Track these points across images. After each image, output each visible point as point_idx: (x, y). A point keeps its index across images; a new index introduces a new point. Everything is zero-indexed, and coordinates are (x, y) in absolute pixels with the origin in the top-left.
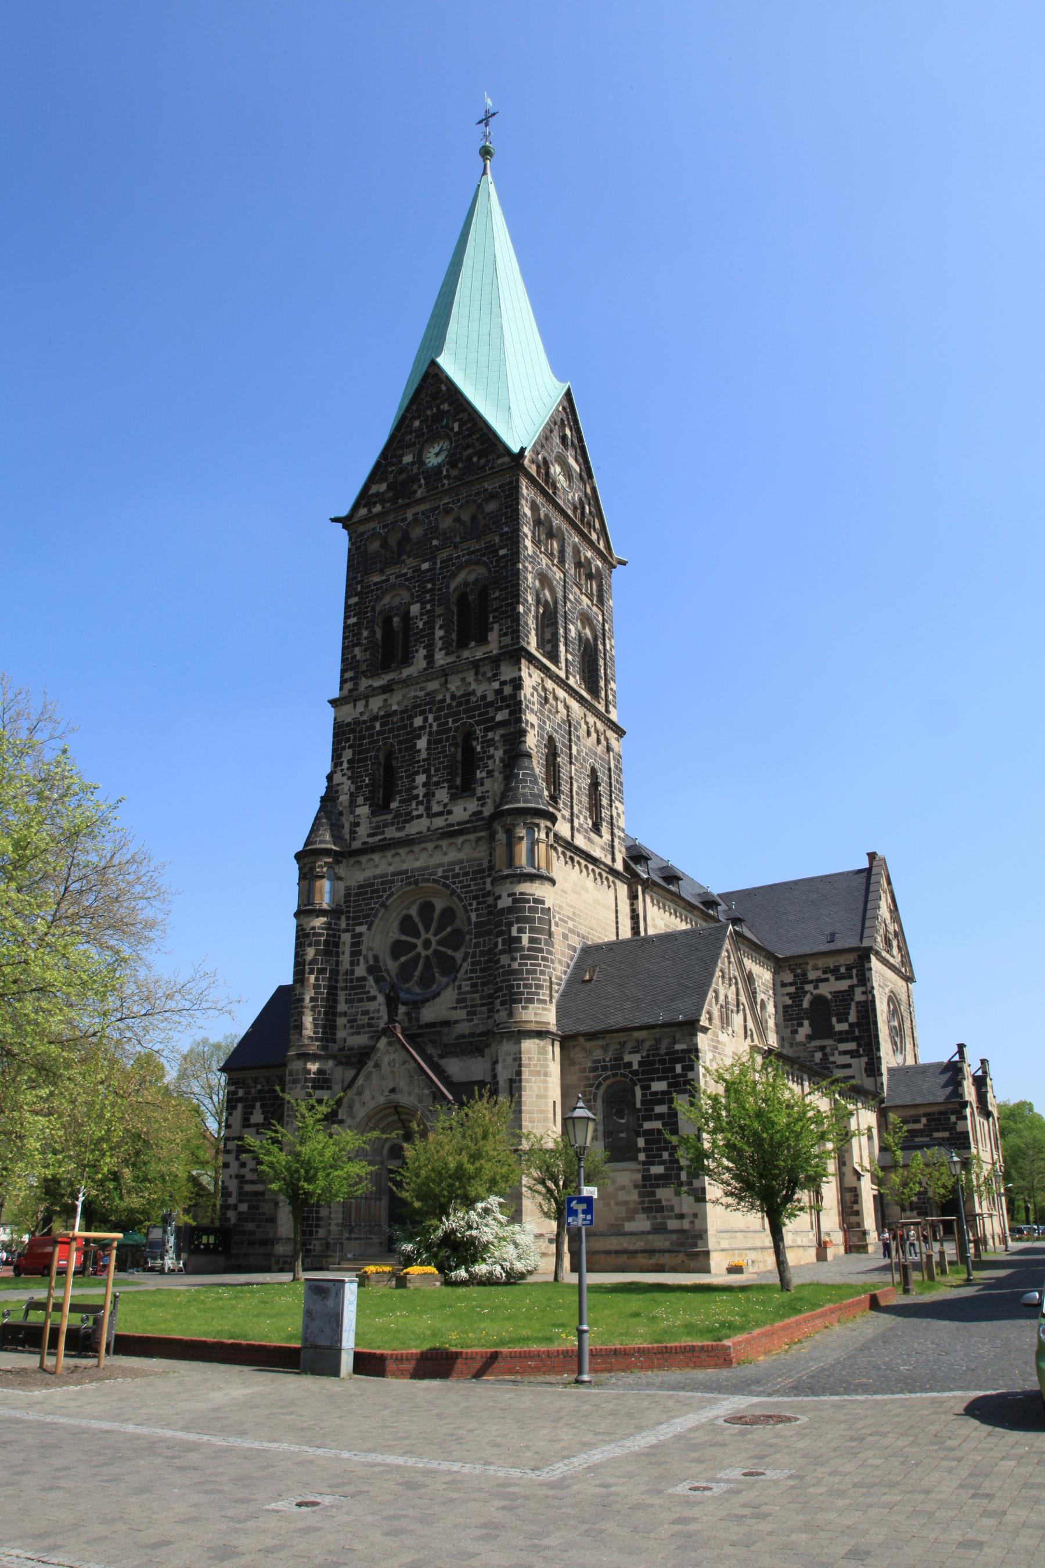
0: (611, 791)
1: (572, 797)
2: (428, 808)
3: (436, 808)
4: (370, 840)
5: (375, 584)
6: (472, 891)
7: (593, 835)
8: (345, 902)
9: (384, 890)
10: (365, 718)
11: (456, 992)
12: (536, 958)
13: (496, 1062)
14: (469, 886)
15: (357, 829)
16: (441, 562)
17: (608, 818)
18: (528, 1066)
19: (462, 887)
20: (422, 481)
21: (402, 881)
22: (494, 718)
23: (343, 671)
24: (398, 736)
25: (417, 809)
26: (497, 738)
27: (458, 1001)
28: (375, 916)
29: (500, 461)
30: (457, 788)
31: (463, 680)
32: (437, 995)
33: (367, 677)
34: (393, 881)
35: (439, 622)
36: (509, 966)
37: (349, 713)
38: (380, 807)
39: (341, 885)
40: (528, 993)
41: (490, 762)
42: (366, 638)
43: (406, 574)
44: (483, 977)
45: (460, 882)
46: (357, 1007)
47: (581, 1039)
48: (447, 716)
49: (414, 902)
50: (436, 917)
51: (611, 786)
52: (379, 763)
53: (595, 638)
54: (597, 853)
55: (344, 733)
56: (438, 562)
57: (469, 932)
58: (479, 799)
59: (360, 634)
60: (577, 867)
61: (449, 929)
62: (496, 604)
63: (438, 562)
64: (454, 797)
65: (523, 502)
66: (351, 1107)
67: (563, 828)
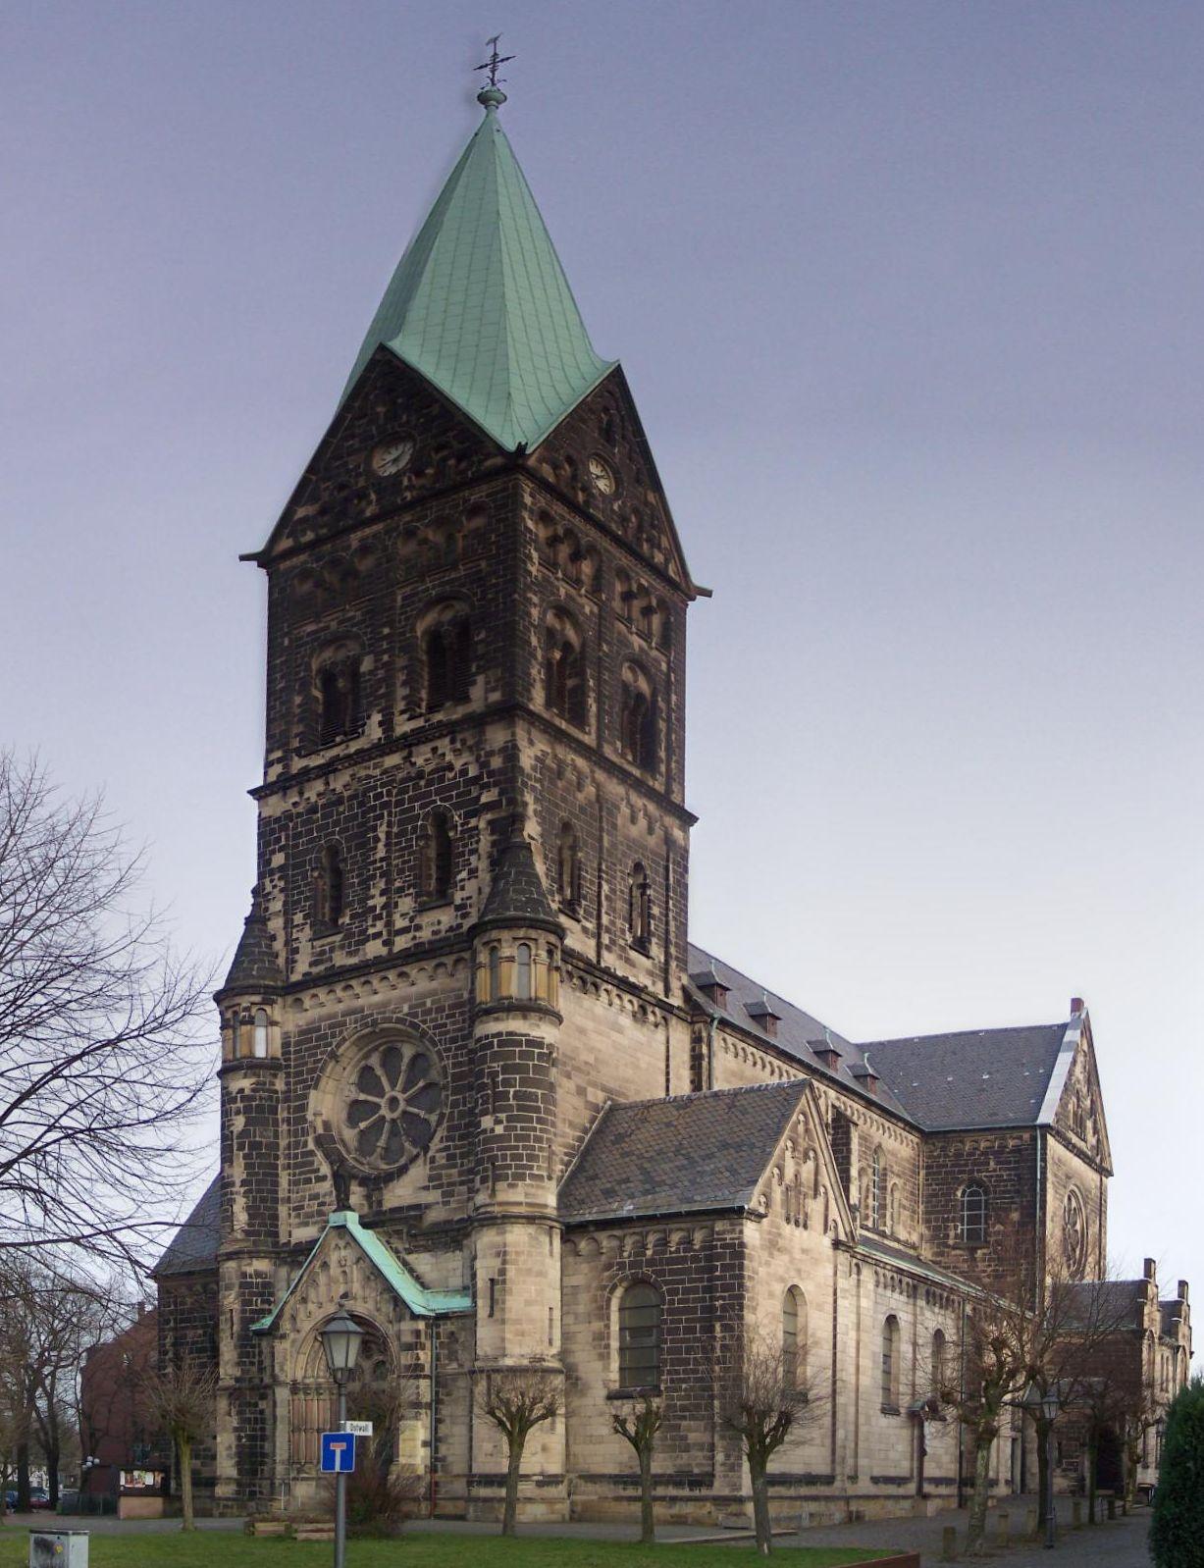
0: (667, 896)
1: (600, 904)
2: (389, 924)
3: (400, 923)
4: (315, 970)
5: (309, 634)
6: (448, 1032)
7: (633, 955)
8: (283, 1054)
9: (333, 1036)
10: (300, 809)
11: (428, 1166)
12: (530, 1119)
13: (474, 1258)
14: (445, 1025)
15: (297, 957)
16: (404, 599)
17: (661, 931)
18: (515, 1262)
19: (435, 1028)
20: (373, 497)
21: (356, 1022)
22: (478, 798)
23: (269, 751)
24: (347, 830)
25: (374, 926)
26: (482, 825)
27: (431, 1179)
28: (322, 1070)
29: (489, 463)
30: (429, 894)
31: (434, 750)
32: (403, 1170)
33: (300, 756)
34: (344, 1024)
35: (401, 677)
36: (493, 1130)
37: (277, 806)
38: (325, 927)
39: (277, 1031)
40: (518, 1167)
41: (473, 859)
42: (299, 706)
43: (353, 617)
44: (463, 1146)
45: (432, 1021)
46: (304, 1190)
47: (592, 1229)
48: (412, 800)
49: (376, 1049)
50: (403, 1068)
51: (667, 890)
52: (323, 869)
53: (654, 694)
54: (641, 979)
55: (273, 831)
56: (399, 598)
57: (445, 1087)
58: (458, 908)
59: (290, 701)
60: (603, 994)
61: (421, 1084)
62: (481, 649)
63: (399, 598)
64: (422, 909)
65: (526, 515)
66: (294, 1318)
67: (578, 941)
